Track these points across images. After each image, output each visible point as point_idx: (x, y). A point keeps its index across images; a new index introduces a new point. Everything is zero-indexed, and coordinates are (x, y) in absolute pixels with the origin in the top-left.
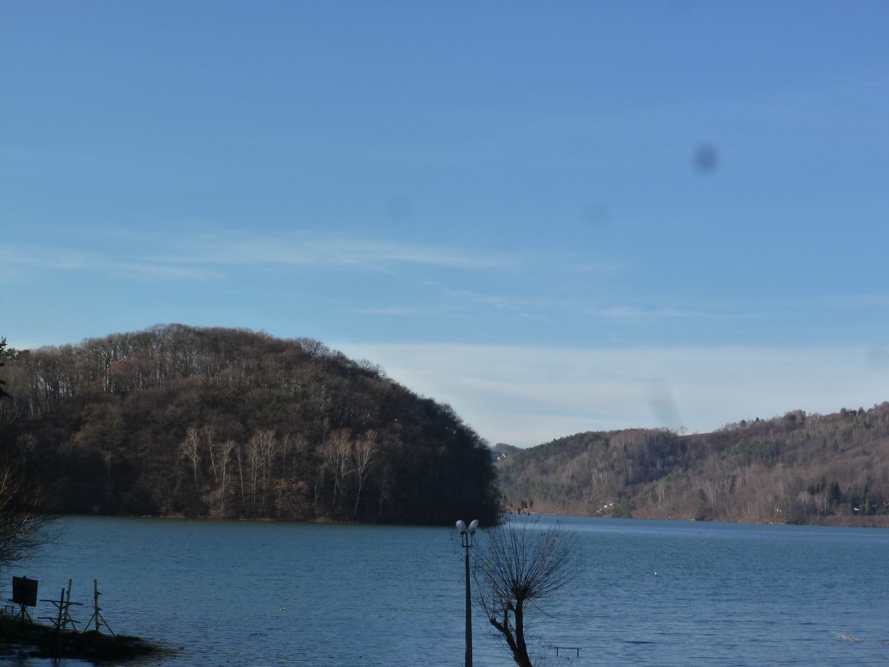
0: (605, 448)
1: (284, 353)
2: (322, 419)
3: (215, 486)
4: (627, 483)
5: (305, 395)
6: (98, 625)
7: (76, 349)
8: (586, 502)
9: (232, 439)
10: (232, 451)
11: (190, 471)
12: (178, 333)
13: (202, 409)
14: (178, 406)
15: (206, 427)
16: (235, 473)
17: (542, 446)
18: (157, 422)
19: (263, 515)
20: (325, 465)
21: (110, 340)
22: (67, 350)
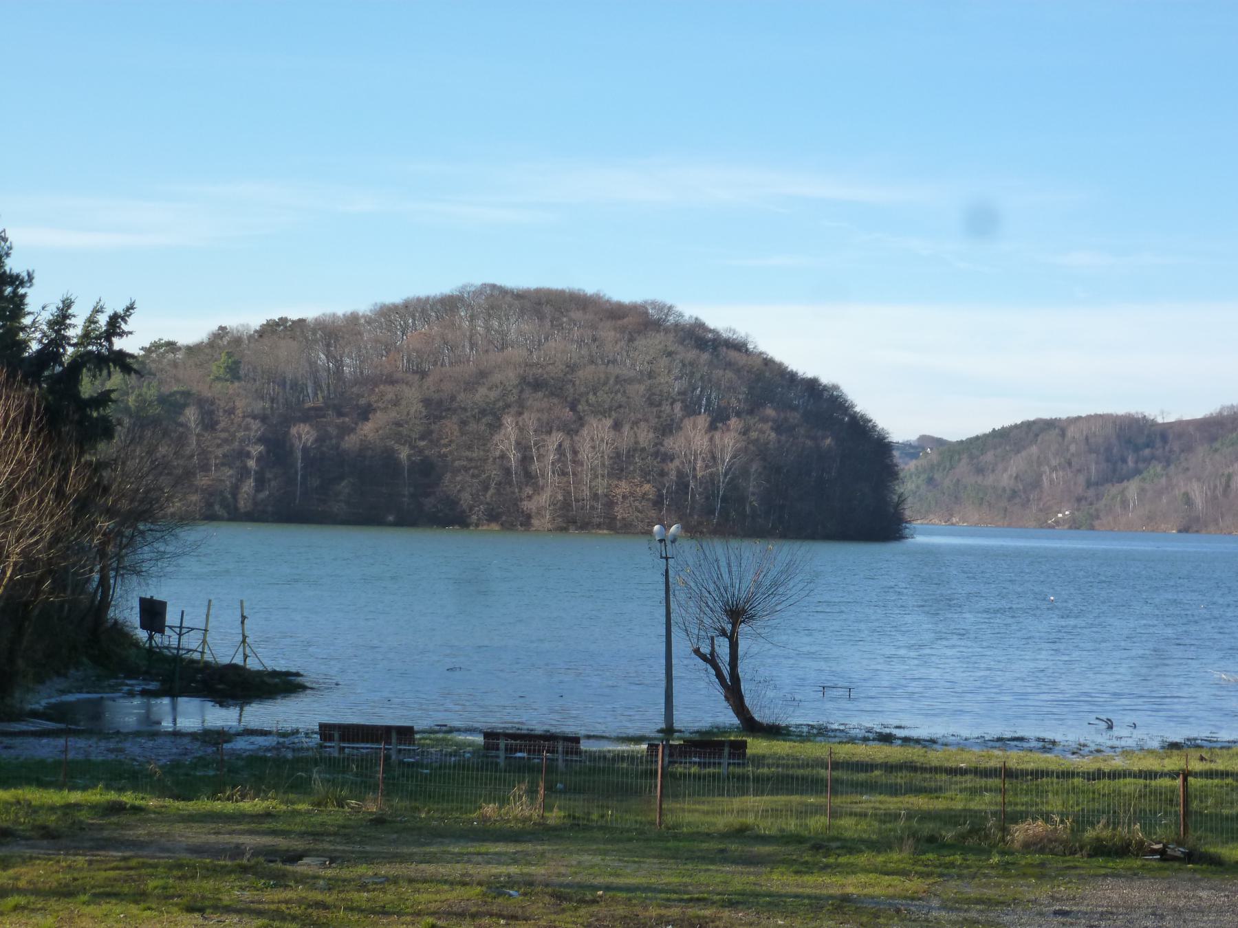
0: (1060, 439)
1: (625, 320)
2: (672, 404)
3: (538, 489)
4: (1089, 484)
5: (651, 375)
6: (246, 657)
7: (364, 316)
8: (1034, 508)
9: (558, 430)
10: (560, 445)
11: (508, 471)
12: (492, 295)
13: (521, 391)
14: (490, 389)
15: (526, 415)
16: (564, 473)
17: (977, 438)
18: (465, 410)
19: (599, 526)
20: (677, 462)
21: (406, 305)
22: (353, 319)
